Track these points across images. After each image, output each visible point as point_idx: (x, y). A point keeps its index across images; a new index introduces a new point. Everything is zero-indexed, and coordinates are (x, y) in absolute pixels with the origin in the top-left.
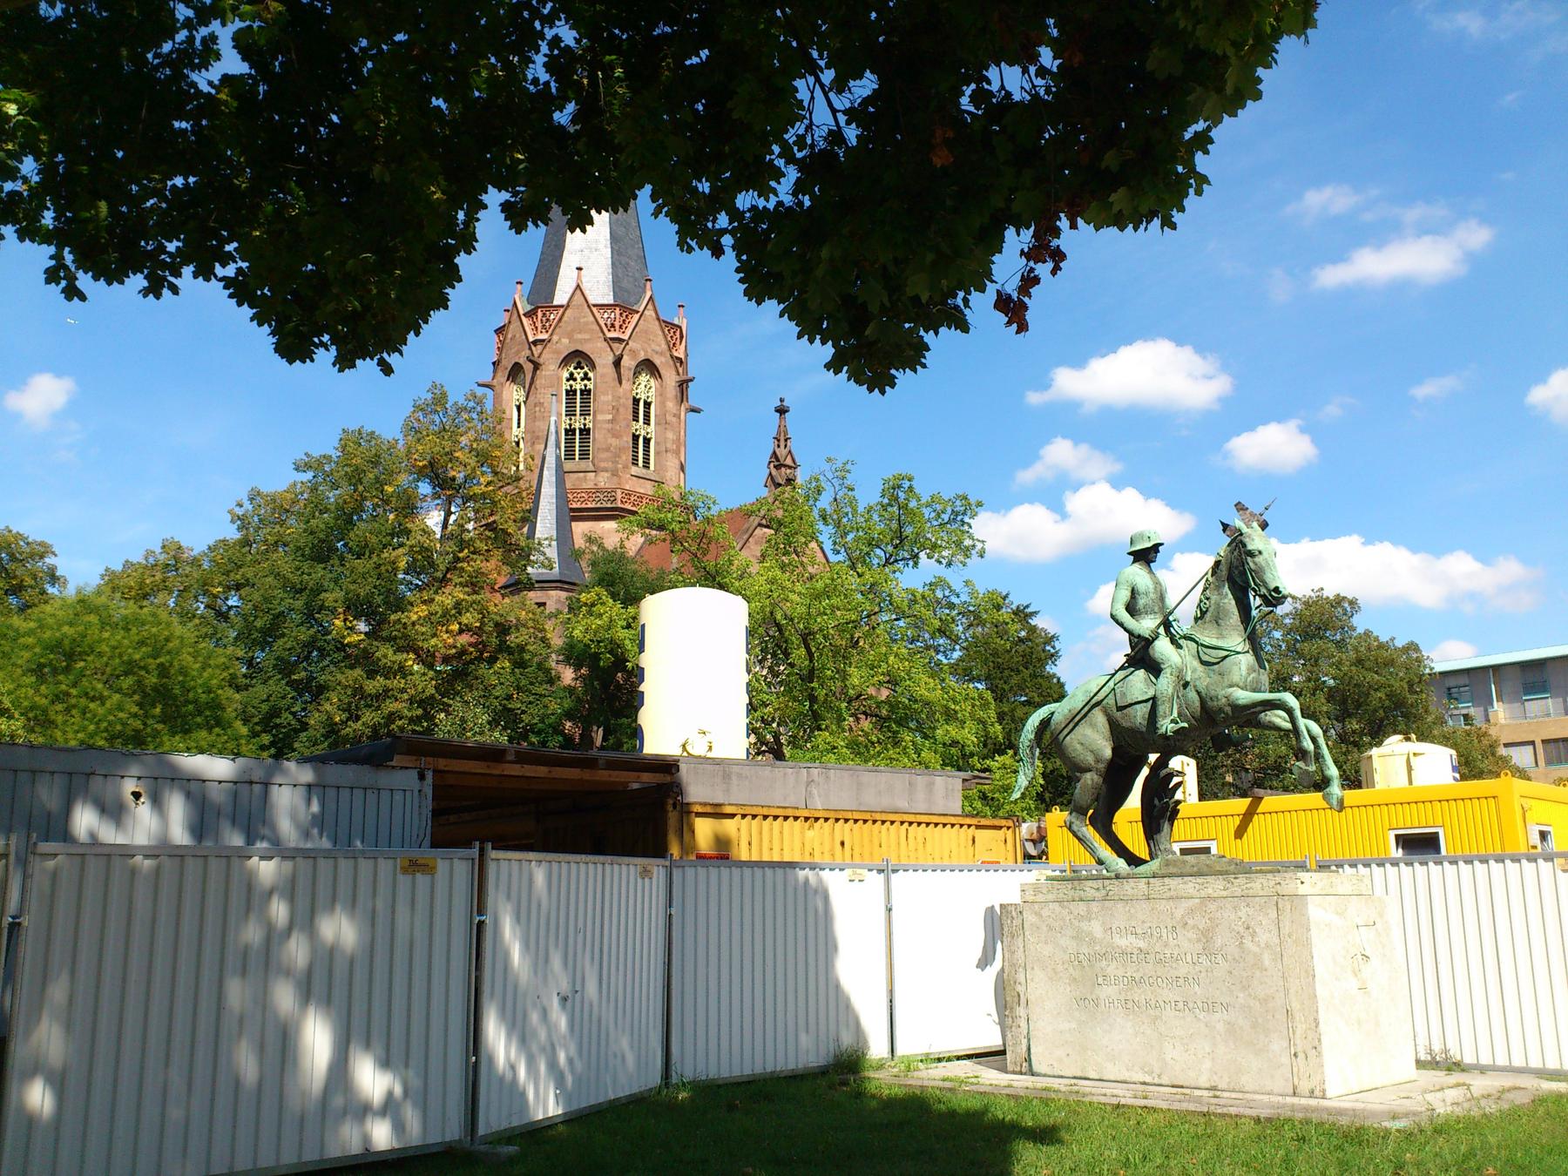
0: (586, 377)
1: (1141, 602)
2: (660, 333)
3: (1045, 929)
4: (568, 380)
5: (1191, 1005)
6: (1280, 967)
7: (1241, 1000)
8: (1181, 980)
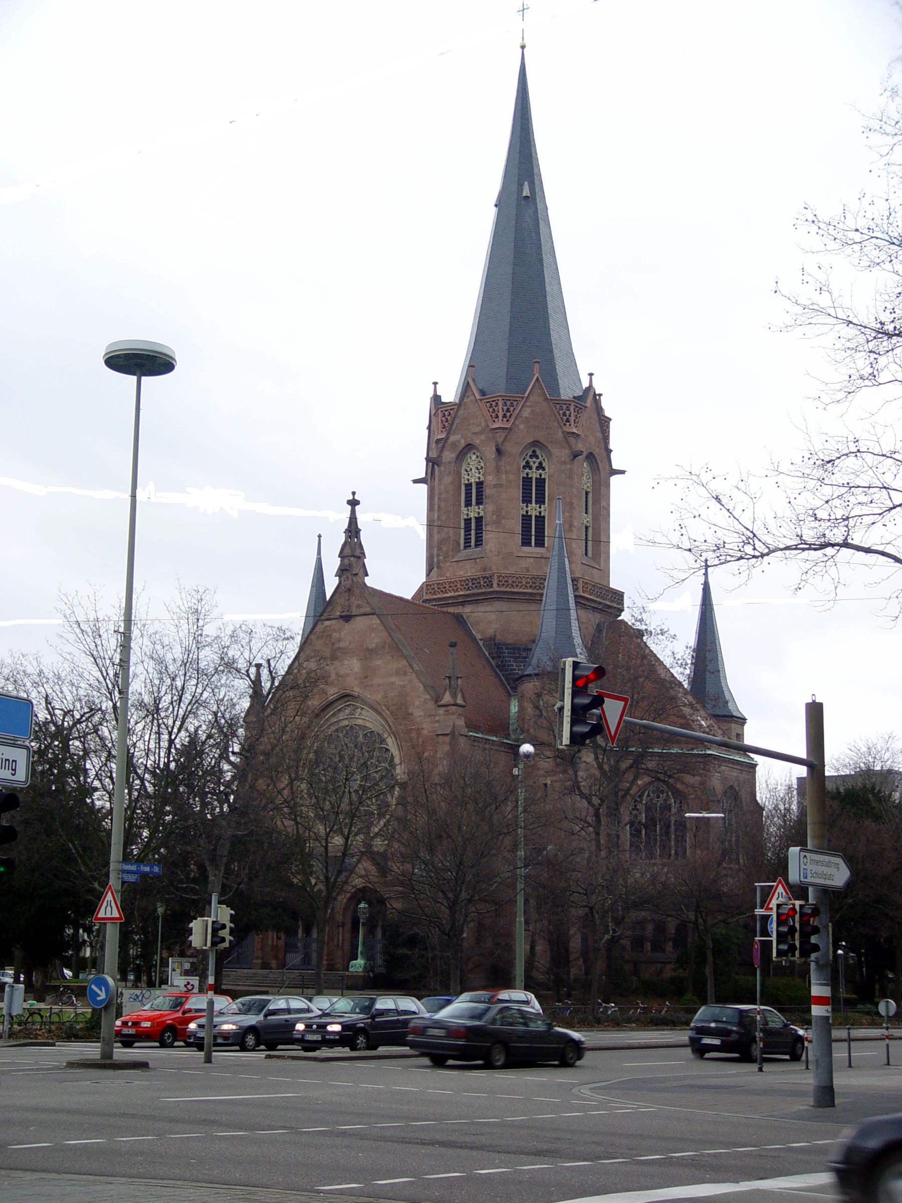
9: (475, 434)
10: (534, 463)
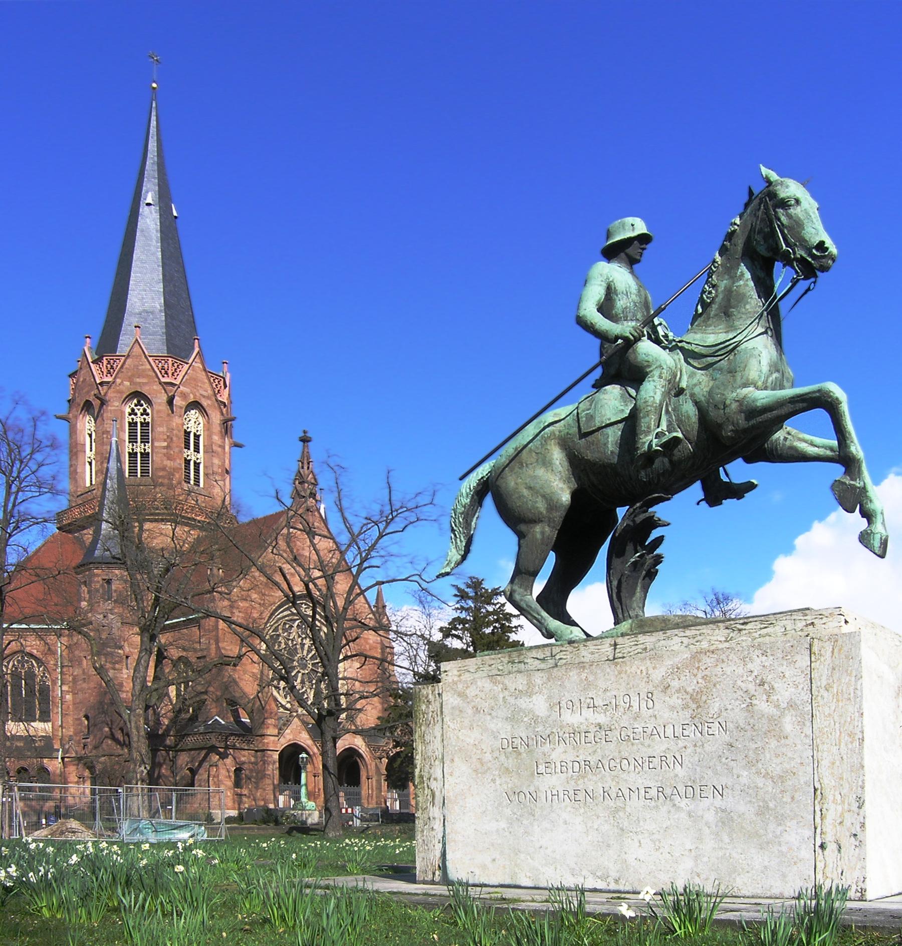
0: (145, 413)
1: (621, 303)
2: (207, 381)
3: (470, 711)
4: (130, 415)
5: (668, 791)
6: (809, 732)
7: (744, 780)
8: (656, 761)
9: (204, 397)
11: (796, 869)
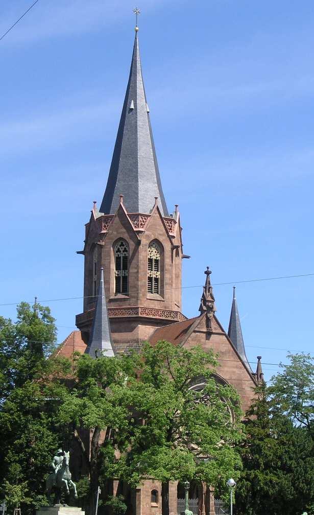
9: (160, 235)
10: (122, 248)
11: (166, 372)
